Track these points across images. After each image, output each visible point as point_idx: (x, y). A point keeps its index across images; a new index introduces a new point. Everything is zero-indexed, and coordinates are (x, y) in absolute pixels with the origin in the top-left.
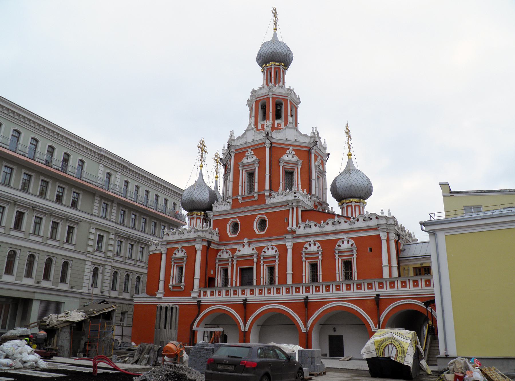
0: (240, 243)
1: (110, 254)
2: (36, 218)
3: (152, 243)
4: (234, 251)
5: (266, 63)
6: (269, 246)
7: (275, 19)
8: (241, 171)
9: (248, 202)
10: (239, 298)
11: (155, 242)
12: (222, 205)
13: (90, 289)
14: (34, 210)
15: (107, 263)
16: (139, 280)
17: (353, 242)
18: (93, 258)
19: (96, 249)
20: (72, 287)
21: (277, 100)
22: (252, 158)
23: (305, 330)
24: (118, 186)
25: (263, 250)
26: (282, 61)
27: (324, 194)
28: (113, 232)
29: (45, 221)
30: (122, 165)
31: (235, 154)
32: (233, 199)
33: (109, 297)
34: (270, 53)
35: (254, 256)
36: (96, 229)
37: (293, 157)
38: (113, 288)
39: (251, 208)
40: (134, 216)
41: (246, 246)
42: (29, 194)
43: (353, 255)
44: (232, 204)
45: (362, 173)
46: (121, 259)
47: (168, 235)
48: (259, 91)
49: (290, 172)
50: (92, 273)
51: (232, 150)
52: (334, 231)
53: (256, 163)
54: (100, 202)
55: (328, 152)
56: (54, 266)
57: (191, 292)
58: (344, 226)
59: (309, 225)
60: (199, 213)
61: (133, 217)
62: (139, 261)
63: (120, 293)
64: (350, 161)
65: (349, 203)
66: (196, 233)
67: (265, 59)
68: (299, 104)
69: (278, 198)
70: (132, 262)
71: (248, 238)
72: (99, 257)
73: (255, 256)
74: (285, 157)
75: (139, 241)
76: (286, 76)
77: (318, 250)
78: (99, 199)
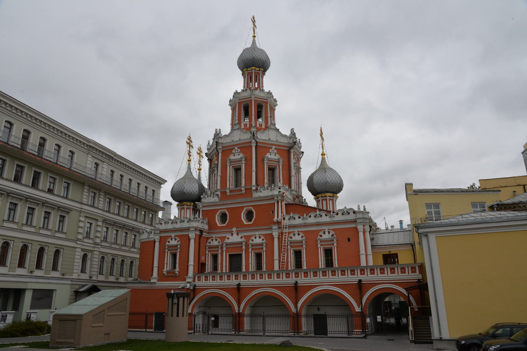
0: (229, 232)
1: (98, 240)
2: (11, 204)
3: (145, 231)
4: (223, 239)
5: (247, 67)
6: (256, 235)
7: (254, 27)
8: (228, 167)
9: (236, 193)
10: (233, 282)
11: (148, 230)
12: (211, 196)
13: (80, 275)
14: (27, 201)
15: (96, 249)
16: (114, 262)
17: (334, 233)
18: (82, 245)
19: (85, 236)
20: (63, 275)
21: (258, 102)
22: (239, 155)
23: (295, 311)
24: (105, 175)
25: (251, 239)
26: (261, 67)
27: (300, 187)
28: (100, 219)
29: (20, 207)
30: (109, 155)
31: (222, 151)
32: (221, 192)
33: (97, 281)
34: (251, 59)
35: (242, 243)
36: (85, 217)
37: (275, 156)
38: (101, 273)
39: (239, 200)
40: (118, 203)
41: (235, 235)
42: (22, 184)
43: (334, 244)
44: (220, 196)
45: (335, 171)
46: (108, 245)
47: (161, 224)
48: (242, 94)
49: (272, 168)
50: (82, 259)
51: (220, 147)
52: (316, 223)
53: (243, 160)
54: (89, 191)
55: (302, 150)
56: (46, 254)
57: (186, 277)
58: (325, 219)
59: (293, 217)
60: (189, 204)
61: (118, 204)
62: (114, 243)
63: (107, 277)
64: (323, 160)
65: (325, 197)
66: (189, 223)
67: (246, 64)
68: (276, 106)
69: (264, 193)
70: (118, 247)
71: (237, 228)
72: (88, 244)
73: (244, 243)
74: (268, 155)
75: (133, 229)
76: (264, 79)
77: (302, 239)
78: (87, 188)
